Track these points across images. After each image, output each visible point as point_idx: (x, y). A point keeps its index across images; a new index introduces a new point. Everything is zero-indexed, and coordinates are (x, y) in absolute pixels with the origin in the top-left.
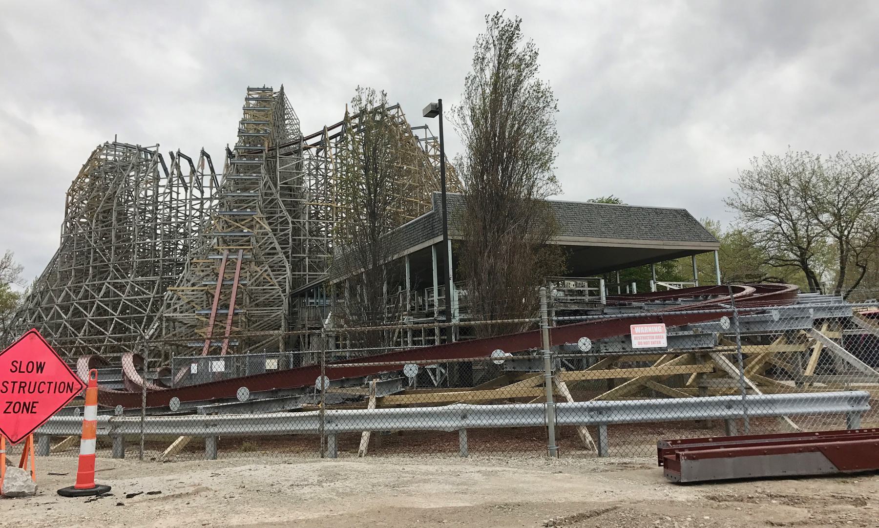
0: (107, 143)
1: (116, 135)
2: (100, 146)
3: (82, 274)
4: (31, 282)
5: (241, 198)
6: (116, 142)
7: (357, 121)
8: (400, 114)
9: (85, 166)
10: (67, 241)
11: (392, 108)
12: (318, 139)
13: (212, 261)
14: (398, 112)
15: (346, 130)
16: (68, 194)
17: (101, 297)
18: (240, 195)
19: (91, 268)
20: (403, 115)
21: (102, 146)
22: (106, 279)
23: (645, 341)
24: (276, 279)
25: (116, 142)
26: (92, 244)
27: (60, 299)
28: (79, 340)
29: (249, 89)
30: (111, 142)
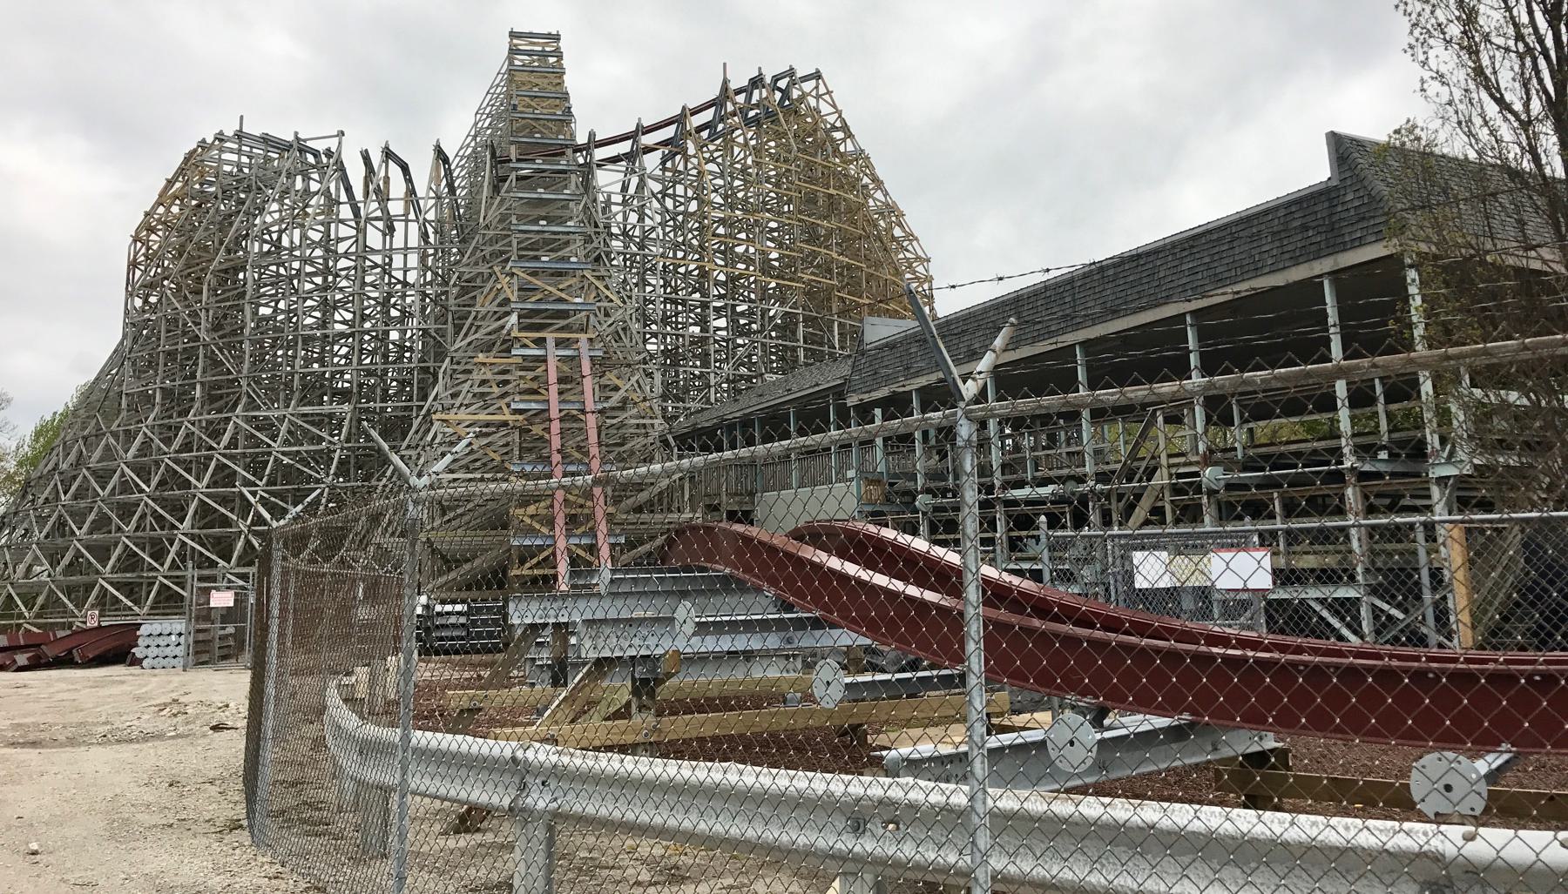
0: (204, 141)
1: (242, 117)
2: (204, 141)
3: (177, 401)
4: (27, 430)
5: (546, 236)
6: (241, 131)
7: (741, 98)
8: (822, 90)
9: (170, 183)
10: (136, 328)
11: (805, 79)
12: (669, 132)
14: (817, 87)
15: (682, 134)
16: (136, 239)
17: (225, 448)
18: (546, 229)
19: (198, 387)
20: (829, 92)
21: (209, 140)
24: (144, 530)
25: (241, 131)
27: (132, 451)
29: (513, 35)
30: (229, 133)
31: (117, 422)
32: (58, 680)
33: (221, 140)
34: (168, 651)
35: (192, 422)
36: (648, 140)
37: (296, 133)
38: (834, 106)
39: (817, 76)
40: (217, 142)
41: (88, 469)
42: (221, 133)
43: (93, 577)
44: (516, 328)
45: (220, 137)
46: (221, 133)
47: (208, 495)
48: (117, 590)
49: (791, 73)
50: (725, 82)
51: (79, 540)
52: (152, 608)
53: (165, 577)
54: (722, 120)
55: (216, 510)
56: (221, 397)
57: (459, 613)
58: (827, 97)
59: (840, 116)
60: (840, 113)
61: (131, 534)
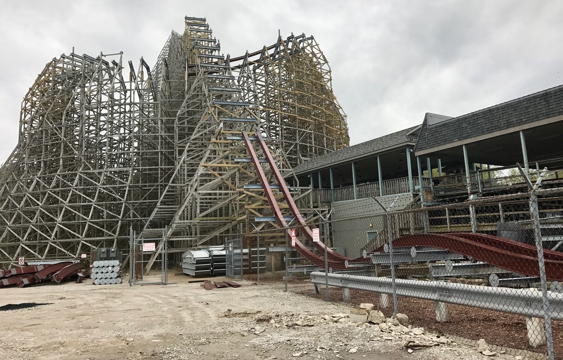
0: (55, 58)
1: (73, 48)
2: (55, 58)
6: (73, 53)
8: (314, 44)
9: (40, 76)
11: (309, 39)
13: (231, 142)
15: (262, 58)
18: (224, 89)
19: (61, 160)
20: (317, 45)
21: (58, 58)
22: (56, 171)
23: (203, 205)
25: (73, 53)
26: (62, 138)
28: (58, 224)
29: (187, 18)
31: (23, 176)
33: (64, 58)
34: (107, 275)
35: (57, 176)
36: (251, 59)
37: (102, 53)
38: (320, 50)
39: (312, 38)
40: (62, 59)
41: (11, 196)
42: (64, 55)
43: (17, 243)
44: (223, 129)
45: (63, 57)
46: (64, 55)
47: (70, 206)
48: (30, 248)
49: (303, 36)
50: (280, 38)
51: (9, 227)
52: (47, 256)
53: (52, 242)
54: (278, 53)
55: (49, 216)
56: (71, 165)
57: (245, 254)
59: (322, 54)
60: (322, 53)
61: (34, 224)
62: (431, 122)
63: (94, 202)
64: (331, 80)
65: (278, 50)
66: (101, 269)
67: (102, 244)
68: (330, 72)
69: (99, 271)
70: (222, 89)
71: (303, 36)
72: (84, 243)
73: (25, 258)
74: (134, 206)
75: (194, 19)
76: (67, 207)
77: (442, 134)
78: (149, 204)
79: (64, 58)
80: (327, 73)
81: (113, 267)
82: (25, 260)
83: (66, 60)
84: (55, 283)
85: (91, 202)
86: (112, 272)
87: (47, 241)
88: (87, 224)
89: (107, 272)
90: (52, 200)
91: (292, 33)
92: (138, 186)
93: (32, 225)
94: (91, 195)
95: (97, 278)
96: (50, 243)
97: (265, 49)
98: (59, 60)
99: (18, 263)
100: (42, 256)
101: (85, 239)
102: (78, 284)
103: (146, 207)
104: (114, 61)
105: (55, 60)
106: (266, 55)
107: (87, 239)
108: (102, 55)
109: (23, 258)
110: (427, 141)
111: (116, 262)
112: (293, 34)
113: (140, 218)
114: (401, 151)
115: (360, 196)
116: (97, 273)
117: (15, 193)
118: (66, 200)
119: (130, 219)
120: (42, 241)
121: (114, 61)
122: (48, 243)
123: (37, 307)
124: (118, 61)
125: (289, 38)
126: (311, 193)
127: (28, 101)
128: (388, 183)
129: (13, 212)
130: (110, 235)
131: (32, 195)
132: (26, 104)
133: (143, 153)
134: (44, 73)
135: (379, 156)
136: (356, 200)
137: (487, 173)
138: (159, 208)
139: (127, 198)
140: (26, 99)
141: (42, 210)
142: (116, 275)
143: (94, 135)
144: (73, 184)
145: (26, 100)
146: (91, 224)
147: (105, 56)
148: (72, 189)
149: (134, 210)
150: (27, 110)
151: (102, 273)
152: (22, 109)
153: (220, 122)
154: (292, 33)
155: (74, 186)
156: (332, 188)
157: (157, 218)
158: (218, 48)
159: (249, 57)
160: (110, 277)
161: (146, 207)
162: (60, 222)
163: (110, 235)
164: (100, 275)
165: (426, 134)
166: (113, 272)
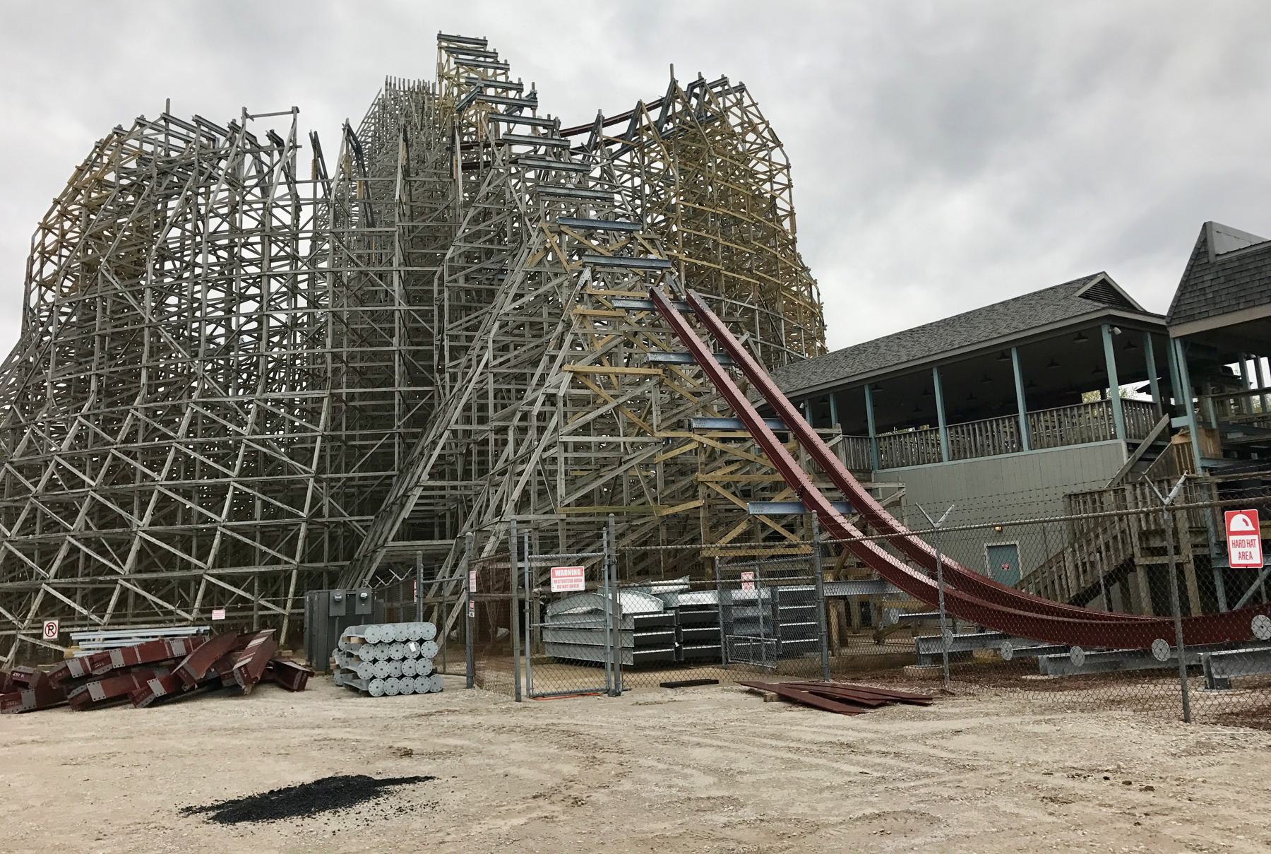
0: (120, 128)
2: (120, 128)
6: (167, 114)
8: (747, 102)
18: (573, 192)
19: (144, 373)
20: (754, 104)
21: (127, 127)
22: (133, 398)
29: (441, 37)
32: (821, 748)
33: (142, 126)
36: (610, 132)
38: (761, 118)
39: (741, 88)
40: (138, 128)
41: (11, 463)
42: (142, 118)
45: (141, 123)
46: (142, 118)
50: (674, 83)
51: (10, 542)
52: (113, 617)
58: (752, 109)
59: (767, 126)
62: (1221, 246)
63: (233, 478)
64: (789, 186)
65: (670, 113)
66: (386, 649)
67: (252, 583)
68: (788, 167)
69: (382, 657)
70: (566, 192)
71: (724, 81)
72: (213, 580)
73: (61, 621)
74: (332, 487)
75: (459, 39)
76: (162, 489)
77: (1263, 276)
78: (361, 483)
79: (142, 126)
80: (782, 169)
81: (421, 641)
82: (61, 627)
83: (147, 131)
84: (235, 692)
85: (227, 476)
86: (417, 659)
87: (114, 577)
88: (218, 533)
89: (404, 659)
90: (120, 474)
91: (700, 73)
92: (338, 438)
93: (72, 536)
94: (226, 457)
95: (374, 677)
96: (121, 581)
97: (641, 108)
98: (130, 133)
99: (40, 636)
100: (102, 617)
101: (215, 571)
102: (296, 694)
103: (352, 490)
104: (272, 131)
105: (118, 131)
106: (645, 122)
107: (220, 571)
108: (246, 115)
109: (56, 622)
110: (1211, 296)
111: (429, 629)
112: (703, 76)
113: (348, 519)
114: (1000, 353)
115: (956, 454)
116: (375, 661)
117: (21, 456)
118: (159, 472)
119: (323, 520)
120: (101, 578)
121: (272, 131)
122: (116, 582)
123: (387, 804)
124: (284, 135)
125: (692, 86)
126: (840, 446)
127: (50, 231)
128: (974, 429)
129: (17, 504)
130: (276, 561)
131: (71, 460)
132: (45, 236)
133: (352, 356)
134: (89, 164)
135: (1017, 348)
136: (946, 463)
137: (1257, 397)
138: (426, 489)
139: (318, 469)
140: (46, 228)
141: (98, 497)
142: (429, 667)
143: (222, 313)
144: (176, 433)
145: (44, 229)
146: (229, 533)
147: (252, 118)
148: (174, 444)
149: (332, 496)
150: (48, 252)
151: (389, 660)
152: (33, 251)
153: (584, 266)
154: (700, 73)
155: (180, 439)
156: (872, 433)
157: (420, 515)
158: (532, 100)
159: (605, 125)
160: (412, 673)
161: (352, 490)
162: (146, 528)
163: (276, 561)
164: (383, 669)
165: (1206, 278)
166: (420, 657)
